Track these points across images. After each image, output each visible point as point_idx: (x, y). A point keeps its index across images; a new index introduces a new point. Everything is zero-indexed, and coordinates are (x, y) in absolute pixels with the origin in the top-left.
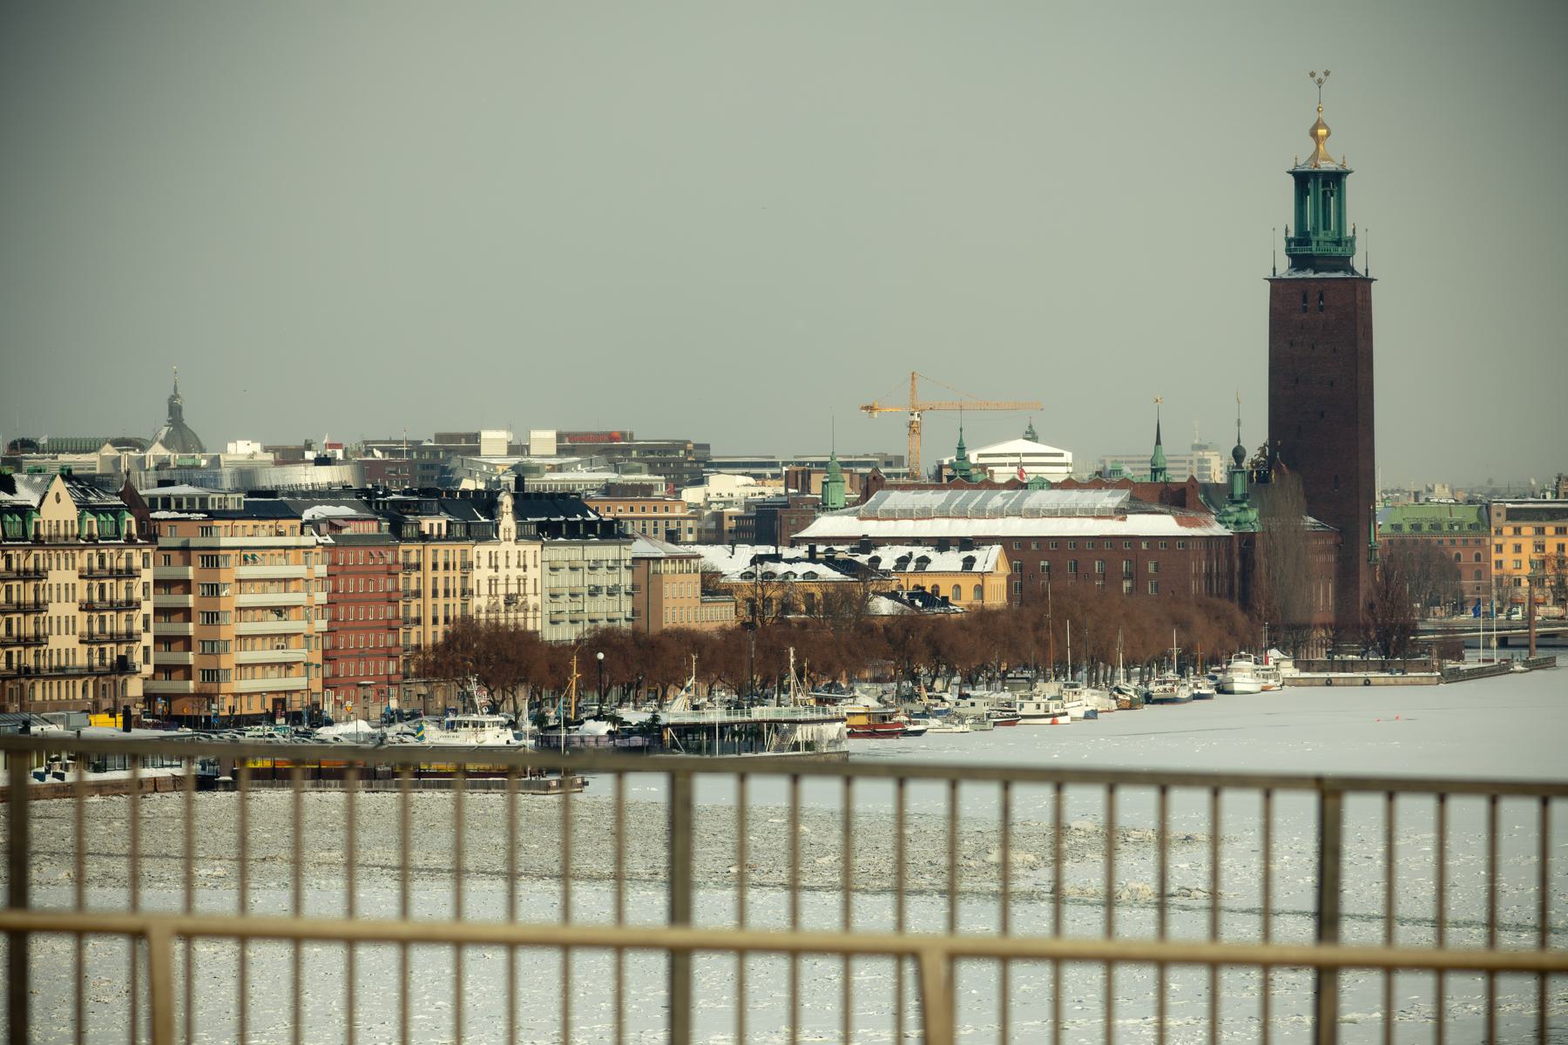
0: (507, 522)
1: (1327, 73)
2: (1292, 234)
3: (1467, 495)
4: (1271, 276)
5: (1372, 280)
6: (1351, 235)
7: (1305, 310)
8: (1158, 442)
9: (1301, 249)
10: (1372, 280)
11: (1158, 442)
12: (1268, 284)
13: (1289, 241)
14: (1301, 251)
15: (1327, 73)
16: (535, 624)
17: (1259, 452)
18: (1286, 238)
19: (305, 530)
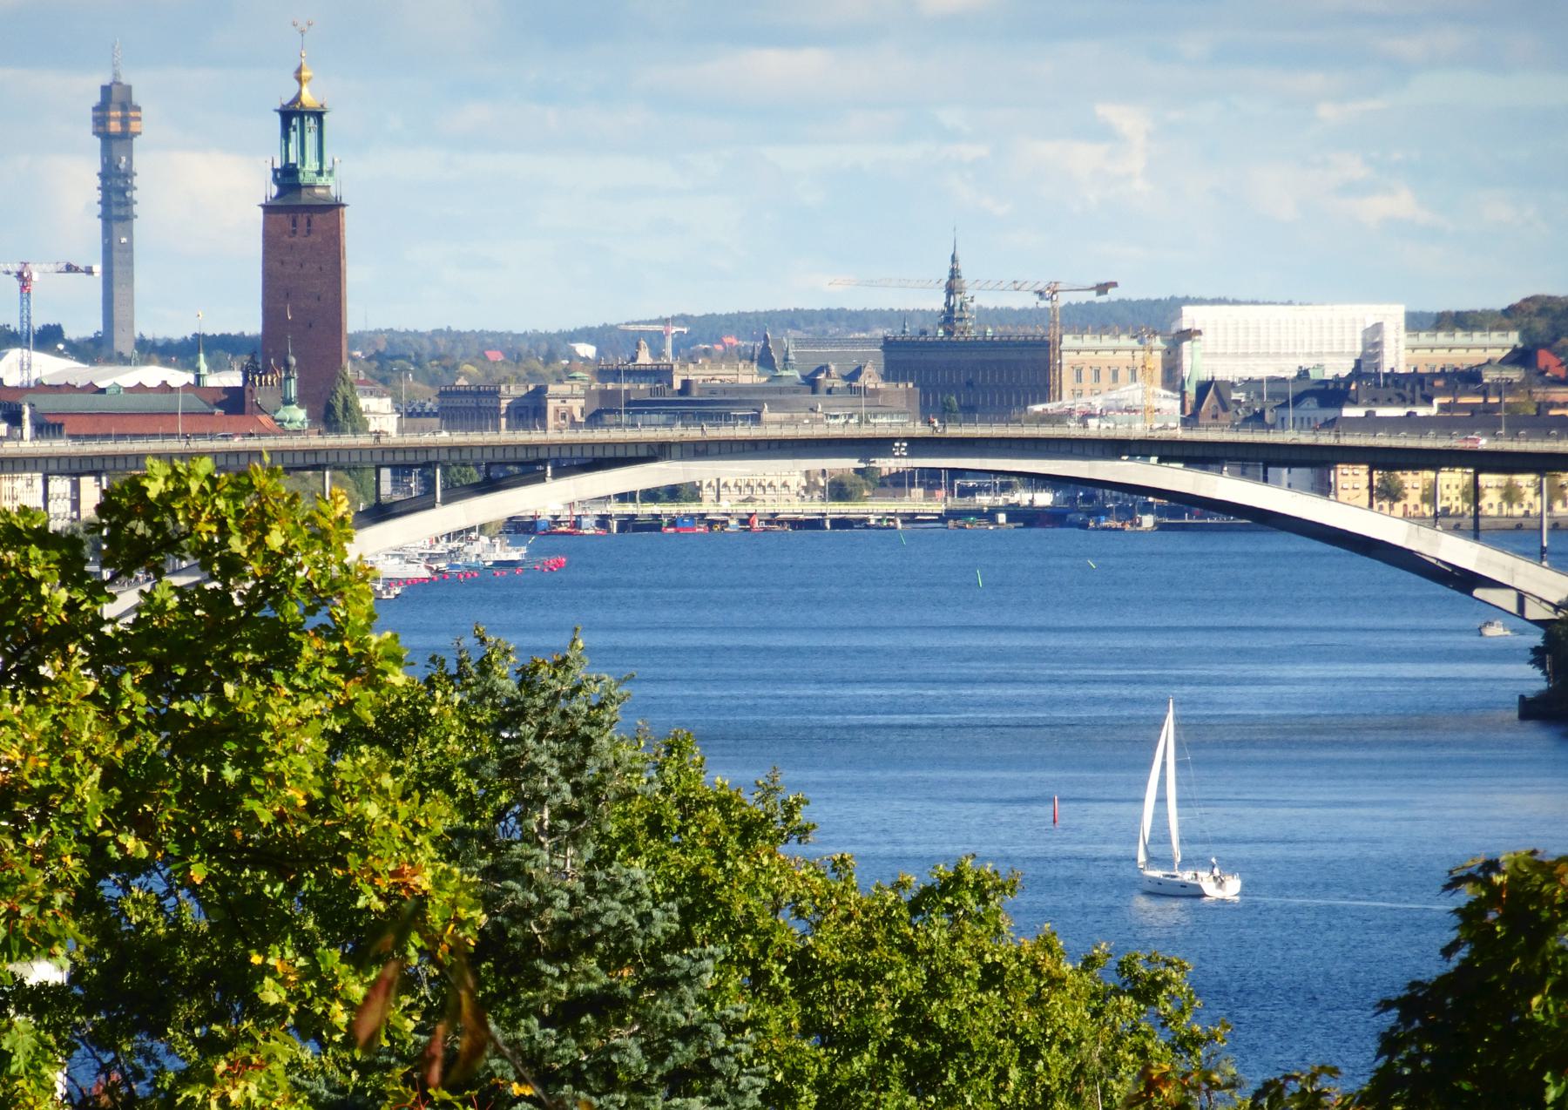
0: (27, 429)
5: (344, 205)
9: (287, 177)
12: (261, 210)
13: (275, 171)
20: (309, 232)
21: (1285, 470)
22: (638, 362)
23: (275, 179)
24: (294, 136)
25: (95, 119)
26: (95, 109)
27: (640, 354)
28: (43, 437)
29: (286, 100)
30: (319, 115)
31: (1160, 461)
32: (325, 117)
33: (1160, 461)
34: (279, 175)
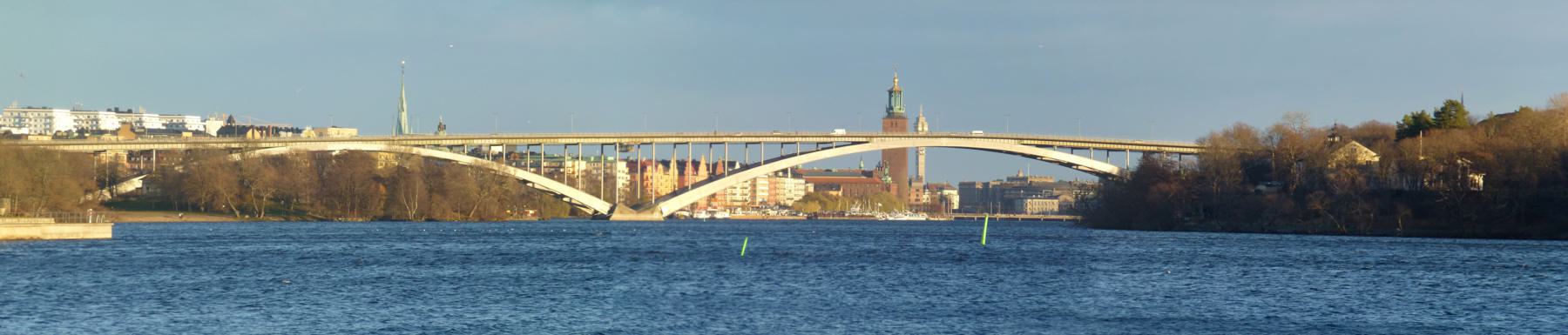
0: (789, 174)
24: (893, 99)
33: (974, 184)
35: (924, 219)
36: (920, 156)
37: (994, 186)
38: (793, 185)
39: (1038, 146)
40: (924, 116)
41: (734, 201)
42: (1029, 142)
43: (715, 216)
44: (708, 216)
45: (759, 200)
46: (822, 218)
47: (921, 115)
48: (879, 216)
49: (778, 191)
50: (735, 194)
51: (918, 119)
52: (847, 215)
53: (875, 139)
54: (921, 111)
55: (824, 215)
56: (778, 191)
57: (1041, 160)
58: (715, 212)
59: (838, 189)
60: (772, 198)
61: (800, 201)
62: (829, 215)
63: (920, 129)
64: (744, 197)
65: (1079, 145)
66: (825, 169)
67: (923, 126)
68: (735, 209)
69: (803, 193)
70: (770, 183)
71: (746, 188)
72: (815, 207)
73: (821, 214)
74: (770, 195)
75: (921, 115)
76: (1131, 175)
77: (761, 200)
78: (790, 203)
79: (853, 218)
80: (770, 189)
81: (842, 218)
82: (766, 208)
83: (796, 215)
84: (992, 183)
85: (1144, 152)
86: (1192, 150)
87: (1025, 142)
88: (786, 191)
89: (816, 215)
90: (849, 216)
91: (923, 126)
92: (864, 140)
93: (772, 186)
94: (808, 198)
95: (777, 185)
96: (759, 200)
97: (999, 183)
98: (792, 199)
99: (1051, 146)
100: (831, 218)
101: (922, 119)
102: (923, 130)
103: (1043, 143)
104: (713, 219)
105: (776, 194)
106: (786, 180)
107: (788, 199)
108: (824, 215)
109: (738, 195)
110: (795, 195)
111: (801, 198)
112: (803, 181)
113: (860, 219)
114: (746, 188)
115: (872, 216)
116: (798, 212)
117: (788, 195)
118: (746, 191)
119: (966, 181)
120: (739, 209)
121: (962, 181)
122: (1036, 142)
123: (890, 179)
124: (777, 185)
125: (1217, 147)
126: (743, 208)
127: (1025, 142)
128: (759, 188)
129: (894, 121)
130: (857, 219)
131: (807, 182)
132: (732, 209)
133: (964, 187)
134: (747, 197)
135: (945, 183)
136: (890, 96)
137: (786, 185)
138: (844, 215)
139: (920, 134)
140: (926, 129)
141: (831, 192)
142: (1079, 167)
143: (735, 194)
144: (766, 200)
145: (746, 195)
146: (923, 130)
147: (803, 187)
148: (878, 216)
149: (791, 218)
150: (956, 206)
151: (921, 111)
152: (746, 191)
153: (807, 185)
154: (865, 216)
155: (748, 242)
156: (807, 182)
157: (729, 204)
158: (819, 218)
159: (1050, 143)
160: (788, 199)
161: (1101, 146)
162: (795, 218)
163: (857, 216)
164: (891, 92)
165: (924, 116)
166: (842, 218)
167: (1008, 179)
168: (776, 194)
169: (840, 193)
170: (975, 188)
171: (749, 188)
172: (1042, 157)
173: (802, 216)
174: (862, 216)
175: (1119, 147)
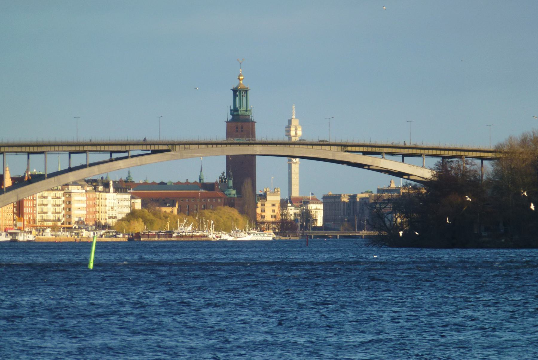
0: (111, 188)
1: (243, 60)
2: (232, 108)
3: (214, 212)
4: (227, 121)
5: (255, 122)
6: (250, 108)
7: (237, 131)
8: (201, 171)
9: (234, 111)
10: (255, 122)
11: (201, 171)
12: (226, 123)
13: (231, 110)
14: (235, 113)
15: (243, 60)
16: (126, 206)
17: (222, 174)
18: (230, 109)
19: (45, 196)
20: (242, 131)
21: (60, 170)
22: (391, 187)
23: (231, 114)
24: (237, 98)
25: (286, 131)
26: (286, 127)
27: (392, 184)
28: (119, 192)
29: (235, 86)
30: (246, 91)
31: (339, 196)
32: (248, 92)
33: (339, 196)
34: (232, 112)
35: (270, 238)
36: (293, 165)
37: (362, 199)
38: (116, 202)
39: (365, 153)
40: (296, 118)
41: (45, 220)
42: (354, 149)
43: (17, 238)
44: (9, 239)
45: (74, 219)
46: (146, 239)
47: (294, 117)
48: (212, 236)
49: (97, 208)
50: (45, 213)
51: (290, 122)
52: (174, 235)
53: (177, 147)
54: (294, 111)
55: (148, 236)
56: (97, 208)
57: (369, 169)
58: (16, 234)
59: (173, 205)
60: (90, 217)
61: (123, 220)
62: (154, 236)
63: (292, 133)
64: (57, 216)
65: (410, 151)
66: (159, 182)
67: (296, 130)
68: (43, 231)
69: (128, 211)
70: (88, 199)
71: (59, 205)
72: (139, 227)
73: (144, 235)
74: (88, 213)
75: (294, 117)
76: (360, 199)
77: (77, 219)
78: (111, 222)
79: (182, 239)
80: (88, 206)
81: (169, 239)
82: (79, 228)
83: (115, 236)
84: (360, 196)
85: (443, 157)
86: (490, 155)
87: (350, 149)
88: (107, 208)
89: (138, 235)
90: (177, 237)
91: (296, 130)
92: (165, 148)
93: (91, 203)
94: (133, 215)
95: (97, 202)
96: (74, 219)
97: (367, 195)
98: (115, 217)
99: (379, 153)
100: (156, 239)
101: (295, 122)
102: (296, 133)
103: (370, 149)
104: (14, 241)
105: (96, 212)
106: (107, 195)
107: (110, 217)
108: (148, 236)
109: (50, 214)
110: (119, 213)
111: (124, 216)
112: (128, 196)
113: (191, 239)
114: (59, 205)
115: (204, 236)
116: (118, 233)
117: (111, 213)
118: (58, 209)
119: (331, 193)
120: (48, 230)
121: (326, 193)
122: (362, 149)
123: (234, 192)
124: (97, 202)
125: (512, 146)
126: (54, 228)
127: (350, 149)
128: (74, 205)
129: (240, 125)
130: (186, 239)
131: (132, 198)
132: (41, 230)
133: (328, 200)
134: (61, 216)
135: (311, 196)
136: (235, 96)
137: (107, 202)
138: (171, 236)
139: (294, 139)
140: (300, 133)
141: (164, 209)
142: (411, 177)
143: (45, 213)
144: (82, 219)
145: (59, 213)
146: (296, 133)
147: (128, 203)
148: (210, 237)
149: (109, 240)
150: (320, 223)
151: (294, 111)
152: (58, 209)
153: (133, 201)
154: (196, 236)
155: (87, 261)
156: (132, 198)
157: (38, 224)
158: (142, 239)
159: (378, 150)
160: (110, 217)
161: (434, 152)
162: (114, 239)
163: (186, 236)
164: (235, 91)
165: (296, 118)
166: (169, 239)
167: (379, 191)
168: (96, 212)
169: (175, 210)
170: (341, 202)
171: (63, 205)
172: (369, 166)
173: (121, 237)
174: (192, 237)
175: (414, 151)
